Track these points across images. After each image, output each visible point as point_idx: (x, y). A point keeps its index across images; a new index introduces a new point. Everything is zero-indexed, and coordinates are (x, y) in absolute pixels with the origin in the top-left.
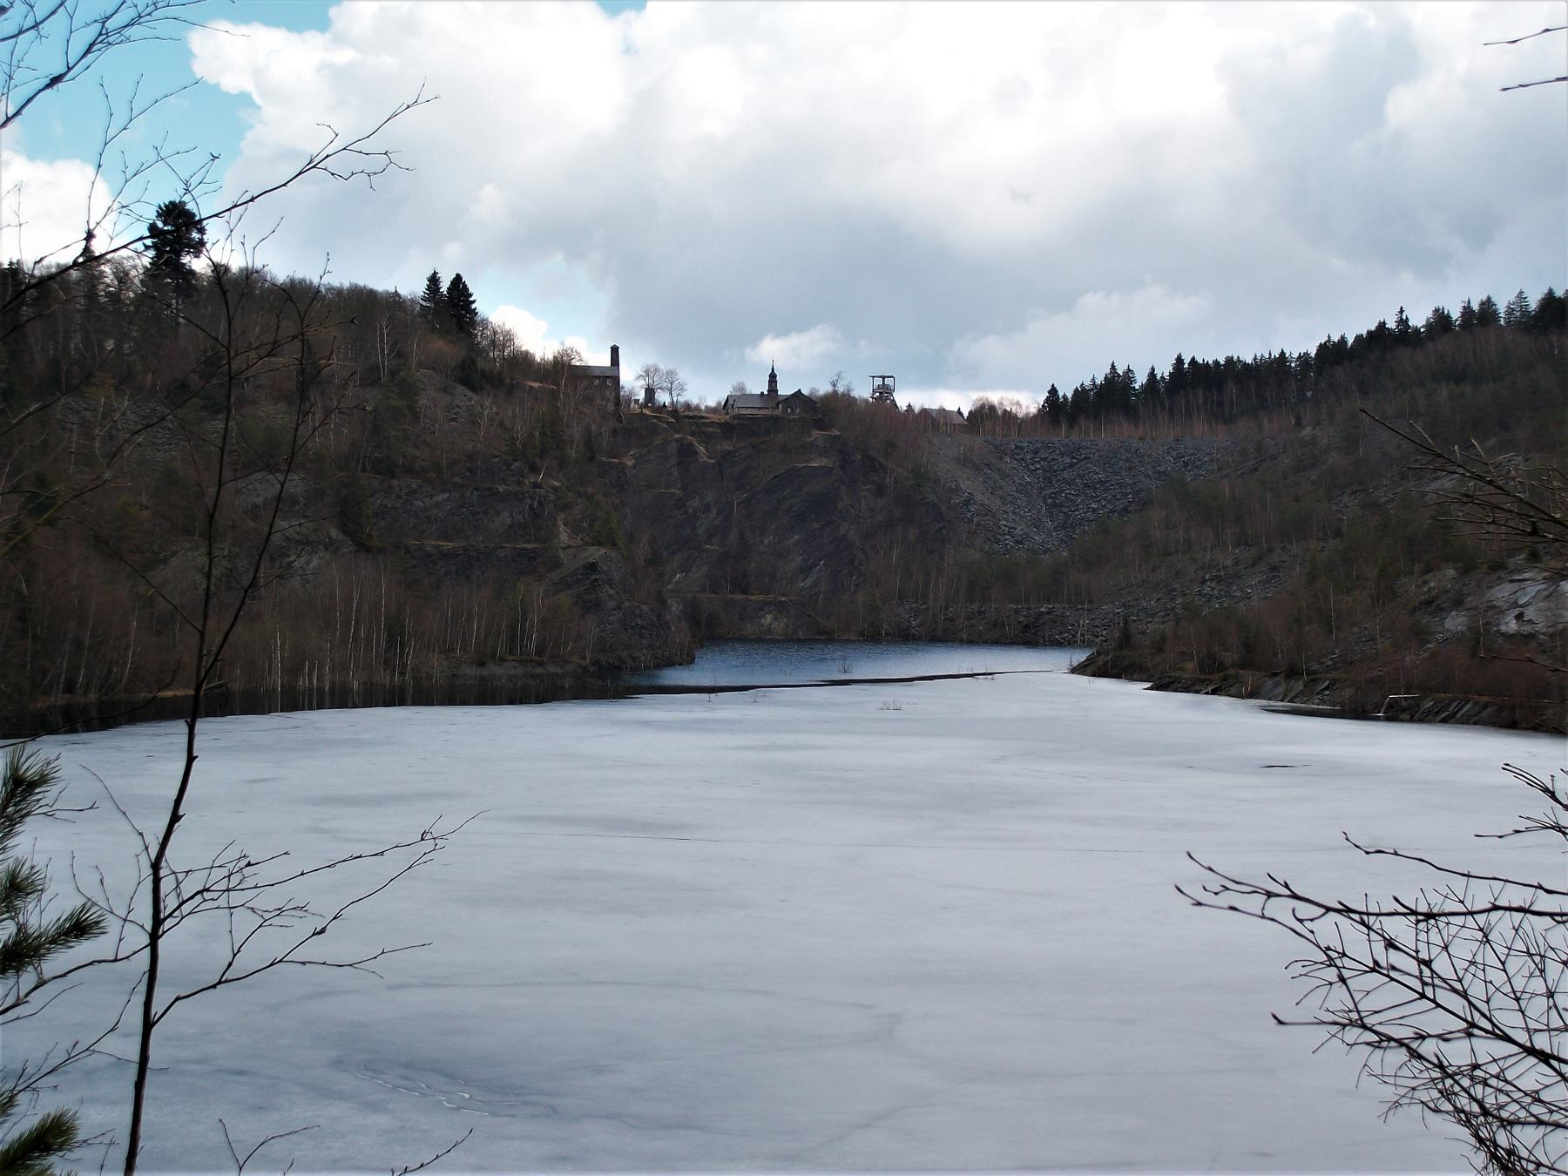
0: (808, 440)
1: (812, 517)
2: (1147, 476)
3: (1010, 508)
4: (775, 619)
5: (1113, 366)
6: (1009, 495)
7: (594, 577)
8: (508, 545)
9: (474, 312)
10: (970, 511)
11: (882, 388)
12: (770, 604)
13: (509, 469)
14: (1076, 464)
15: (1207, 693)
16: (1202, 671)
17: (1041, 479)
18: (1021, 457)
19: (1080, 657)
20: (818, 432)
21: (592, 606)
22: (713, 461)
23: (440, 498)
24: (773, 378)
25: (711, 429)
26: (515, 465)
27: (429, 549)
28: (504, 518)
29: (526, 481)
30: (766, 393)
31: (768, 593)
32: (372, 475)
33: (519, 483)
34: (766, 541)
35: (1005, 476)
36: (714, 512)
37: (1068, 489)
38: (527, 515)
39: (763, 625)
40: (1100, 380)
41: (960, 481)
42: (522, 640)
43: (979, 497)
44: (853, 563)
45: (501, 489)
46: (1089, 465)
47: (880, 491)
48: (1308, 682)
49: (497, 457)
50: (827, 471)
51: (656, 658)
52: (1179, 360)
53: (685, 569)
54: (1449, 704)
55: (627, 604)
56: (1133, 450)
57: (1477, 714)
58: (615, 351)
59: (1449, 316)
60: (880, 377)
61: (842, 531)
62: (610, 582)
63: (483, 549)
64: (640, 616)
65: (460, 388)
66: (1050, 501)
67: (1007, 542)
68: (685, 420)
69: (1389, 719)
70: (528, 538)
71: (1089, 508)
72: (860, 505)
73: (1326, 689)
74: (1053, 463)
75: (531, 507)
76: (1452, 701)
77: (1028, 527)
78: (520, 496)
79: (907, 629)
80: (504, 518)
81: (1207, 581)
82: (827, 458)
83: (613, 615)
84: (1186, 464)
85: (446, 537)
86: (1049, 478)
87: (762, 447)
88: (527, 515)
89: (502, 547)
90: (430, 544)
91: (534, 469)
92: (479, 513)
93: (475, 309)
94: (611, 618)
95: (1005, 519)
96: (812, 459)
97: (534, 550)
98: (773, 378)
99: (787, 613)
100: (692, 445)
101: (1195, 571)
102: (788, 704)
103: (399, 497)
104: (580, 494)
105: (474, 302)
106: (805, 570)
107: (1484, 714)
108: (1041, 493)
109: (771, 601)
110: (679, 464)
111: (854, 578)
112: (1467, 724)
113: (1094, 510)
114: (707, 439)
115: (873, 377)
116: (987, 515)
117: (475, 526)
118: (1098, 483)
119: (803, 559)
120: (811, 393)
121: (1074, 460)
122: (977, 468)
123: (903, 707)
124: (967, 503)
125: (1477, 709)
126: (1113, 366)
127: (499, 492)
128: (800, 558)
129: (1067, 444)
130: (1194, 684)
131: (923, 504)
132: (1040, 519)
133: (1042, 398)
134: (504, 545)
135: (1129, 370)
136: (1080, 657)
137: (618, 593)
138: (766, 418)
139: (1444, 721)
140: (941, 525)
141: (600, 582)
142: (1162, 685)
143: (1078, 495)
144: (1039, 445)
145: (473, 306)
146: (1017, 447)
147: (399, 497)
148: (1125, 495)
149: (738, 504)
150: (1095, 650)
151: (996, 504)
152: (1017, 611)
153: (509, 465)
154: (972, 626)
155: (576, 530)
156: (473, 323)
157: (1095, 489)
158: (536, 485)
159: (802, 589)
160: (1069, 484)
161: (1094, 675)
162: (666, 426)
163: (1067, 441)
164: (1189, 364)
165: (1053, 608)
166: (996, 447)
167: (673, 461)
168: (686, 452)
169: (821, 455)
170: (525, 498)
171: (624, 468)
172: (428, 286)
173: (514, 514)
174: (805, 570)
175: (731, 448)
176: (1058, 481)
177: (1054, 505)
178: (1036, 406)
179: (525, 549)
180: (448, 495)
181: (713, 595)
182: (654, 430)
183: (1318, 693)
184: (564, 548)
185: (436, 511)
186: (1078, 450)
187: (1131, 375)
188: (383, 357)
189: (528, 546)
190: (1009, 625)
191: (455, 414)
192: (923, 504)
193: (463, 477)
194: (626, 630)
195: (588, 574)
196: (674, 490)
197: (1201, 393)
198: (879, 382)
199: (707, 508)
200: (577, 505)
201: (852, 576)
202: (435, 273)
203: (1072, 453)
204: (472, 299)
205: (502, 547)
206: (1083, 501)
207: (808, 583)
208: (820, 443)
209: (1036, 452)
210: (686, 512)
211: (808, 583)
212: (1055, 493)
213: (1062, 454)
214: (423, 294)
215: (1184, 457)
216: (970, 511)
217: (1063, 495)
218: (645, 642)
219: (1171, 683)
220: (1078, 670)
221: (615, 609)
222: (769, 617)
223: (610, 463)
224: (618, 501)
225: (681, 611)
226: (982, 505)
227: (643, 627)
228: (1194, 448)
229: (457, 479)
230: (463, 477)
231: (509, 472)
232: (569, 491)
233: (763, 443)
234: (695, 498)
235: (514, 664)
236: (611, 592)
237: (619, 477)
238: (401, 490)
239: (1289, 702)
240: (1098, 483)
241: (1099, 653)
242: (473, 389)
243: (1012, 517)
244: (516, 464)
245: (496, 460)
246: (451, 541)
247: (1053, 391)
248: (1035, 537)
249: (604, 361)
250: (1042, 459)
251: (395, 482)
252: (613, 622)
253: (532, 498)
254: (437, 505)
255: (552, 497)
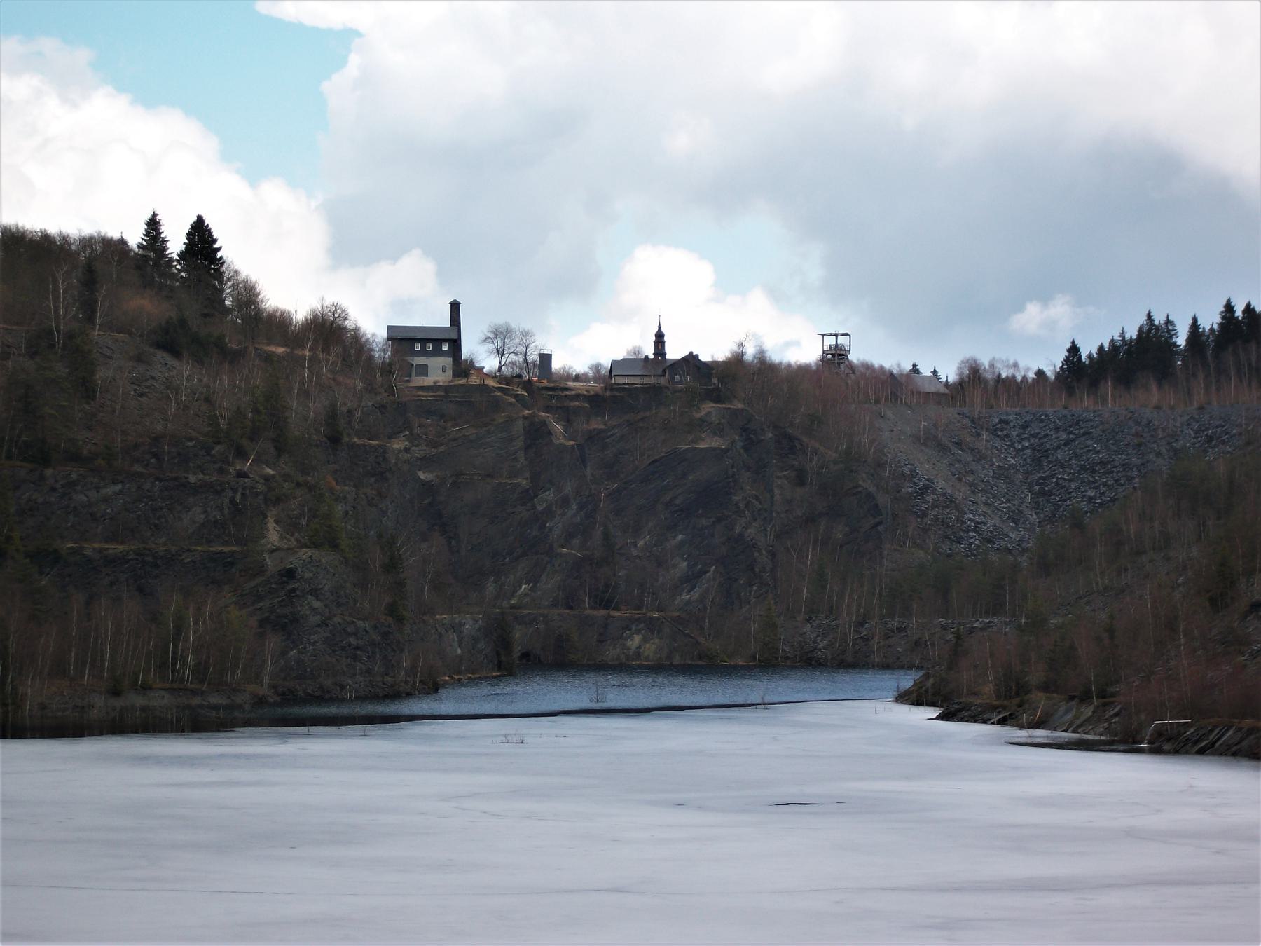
0: (698, 416)
1: (700, 512)
2: (1159, 454)
3: (981, 498)
4: (645, 640)
5: (1149, 317)
6: (983, 481)
7: (291, 586)
8: (199, 548)
9: (220, 262)
10: (926, 502)
11: (834, 350)
12: (639, 620)
13: (208, 454)
14: (1074, 440)
15: (993, 723)
16: (998, 696)
17: (1029, 461)
18: (1005, 433)
19: (907, 681)
20: (714, 405)
21: (286, 625)
22: (572, 443)
23: (110, 490)
24: (660, 338)
25: (577, 403)
26: (218, 448)
27: (89, 553)
28: (194, 515)
29: (231, 469)
30: (651, 356)
31: (639, 608)
32: (18, 463)
33: (221, 471)
34: (641, 543)
35: (980, 457)
36: (574, 506)
37: (1059, 473)
38: (226, 512)
39: (629, 649)
40: (1132, 333)
41: (917, 464)
42: (174, 664)
43: (940, 484)
44: (753, 569)
45: (192, 479)
46: (1089, 442)
47: (800, 479)
48: (1098, 707)
49: (191, 440)
50: (719, 454)
51: (373, 686)
52: (1229, 308)
53: (533, 579)
54: (1211, 731)
55: (337, 619)
56: (1144, 422)
57: (1238, 743)
58: (455, 306)
59: (122, 242)
60: (831, 335)
61: (738, 529)
62: (315, 593)
63: (161, 554)
64: (355, 634)
65: (161, 355)
66: (1037, 488)
67: (972, 540)
68: (544, 392)
69: (1156, 750)
70: (226, 539)
71: (1085, 496)
72: (772, 497)
73: (1116, 715)
74: (1045, 440)
75: (232, 500)
76: (1216, 727)
77: (1003, 521)
78: (219, 488)
79: (812, 651)
80: (194, 515)
81: (1179, 585)
82: (721, 437)
83: (316, 633)
84: (1210, 439)
85: (114, 538)
86: (1039, 460)
87: (641, 424)
88: (226, 512)
89: (189, 550)
90: (91, 548)
91: (241, 454)
92: (161, 508)
93: (221, 258)
94: (314, 637)
95: (972, 512)
96: (703, 440)
97: (232, 553)
98: (660, 338)
99: (658, 633)
100: (544, 423)
101: (1167, 574)
102: (241, 732)
103: (54, 489)
104: (298, 485)
105: (219, 249)
106: (691, 580)
107: (1245, 744)
108: (1027, 479)
109: (639, 618)
110: (527, 448)
111: (755, 588)
112: (1226, 755)
113: (1091, 499)
114: (567, 416)
115: (823, 335)
116: (947, 507)
117: (156, 526)
118: (1097, 464)
119: (688, 565)
120: (858, 360)
121: (1072, 436)
122: (941, 448)
123: (527, 739)
124: (922, 492)
125: (1240, 735)
126: (1149, 317)
127: (189, 483)
128: (685, 564)
129: (1065, 416)
130: (983, 712)
131: (854, 494)
132: (1021, 512)
133: (1064, 354)
134: (194, 548)
135: (1168, 322)
136: (907, 681)
137: (326, 606)
138: (646, 389)
139: (1201, 752)
140: (877, 520)
141: (298, 593)
142: (948, 714)
143: (1070, 480)
144: (1029, 418)
145: (219, 255)
146: (1001, 421)
147: (54, 489)
148: (1130, 479)
149: (606, 497)
150: (921, 673)
151: (961, 492)
152: (944, 627)
153: (208, 451)
154: (889, 646)
155: (290, 526)
156: (219, 274)
157: (1094, 472)
158: (241, 474)
159: (688, 602)
160: (1062, 466)
161: (913, 704)
162: (513, 400)
163: (1065, 412)
164: (1244, 312)
165: (989, 622)
166: (973, 421)
167: (519, 443)
168: (537, 432)
169: (715, 434)
170: (223, 490)
171: (384, 452)
172: (146, 231)
173: (209, 509)
174: (691, 580)
175: (602, 427)
176: (1050, 462)
177: (1042, 493)
178: (1052, 368)
179: (220, 553)
180: (120, 486)
181: (567, 611)
182: (496, 405)
183: (1106, 720)
184: (273, 551)
185: (103, 507)
186: (1078, 423)
187: (1170, 328)
188: (57, 316)
189: (225, 549)
190: (933, 645)
191: (148, 387)
192: (854, 494)
193: (147, 465)
194: (334, 651)
195: (284, 582)
196: (519, 480)
197: (1254, 348)
198: (831, 341)
199: (565, 502)
200: (295, 498)
201: (751, 586)
202: (155, 215)
203: (1070, 426)
204: (176, 243)
205: (189, 550)
206: (1077, 488)
207: (695, 595)
208: (714, 419)
209: (1025, 426)
210: (534, 507)
211: (695, 595)
212: (1044, 479)
213: (1057, 429)
214: (141, 240)
215: (1207, 429)
216: (926, 502)
217: (1054, 480)
218: (359, 665)
219: (959, 710)
220: (904, 698)
221: (319, 626)
222: (637, 639)
223: (364, 445)
224: (374, 492)
225: (479, 630)
226: (944, 494)
227: (357, 648)
228: (1221, 418)
229: (137, 468)
230: (147, 465)
231: (209, 458)
232: (285, 481)
233: (642, 419)
234: (550, 489)
235: (163, 693)
236: (317, 604)
237: (378, 463)
238: (56, 481)
239: (1073, 732)
240: (1097, 464)
241: (927, 676)
242: (177, 354)
243: (983, 508)
244: (218, 448)
245: (190, 444)
246: (123, 543)
247: (1074, 349)
248: (1010, 534)
249: (442, 320)
250: (1033, 436)
251: (49, 472)
252: (316, 642)
253: (234, 490)
254: (106, 500)
255: (260, 488)
